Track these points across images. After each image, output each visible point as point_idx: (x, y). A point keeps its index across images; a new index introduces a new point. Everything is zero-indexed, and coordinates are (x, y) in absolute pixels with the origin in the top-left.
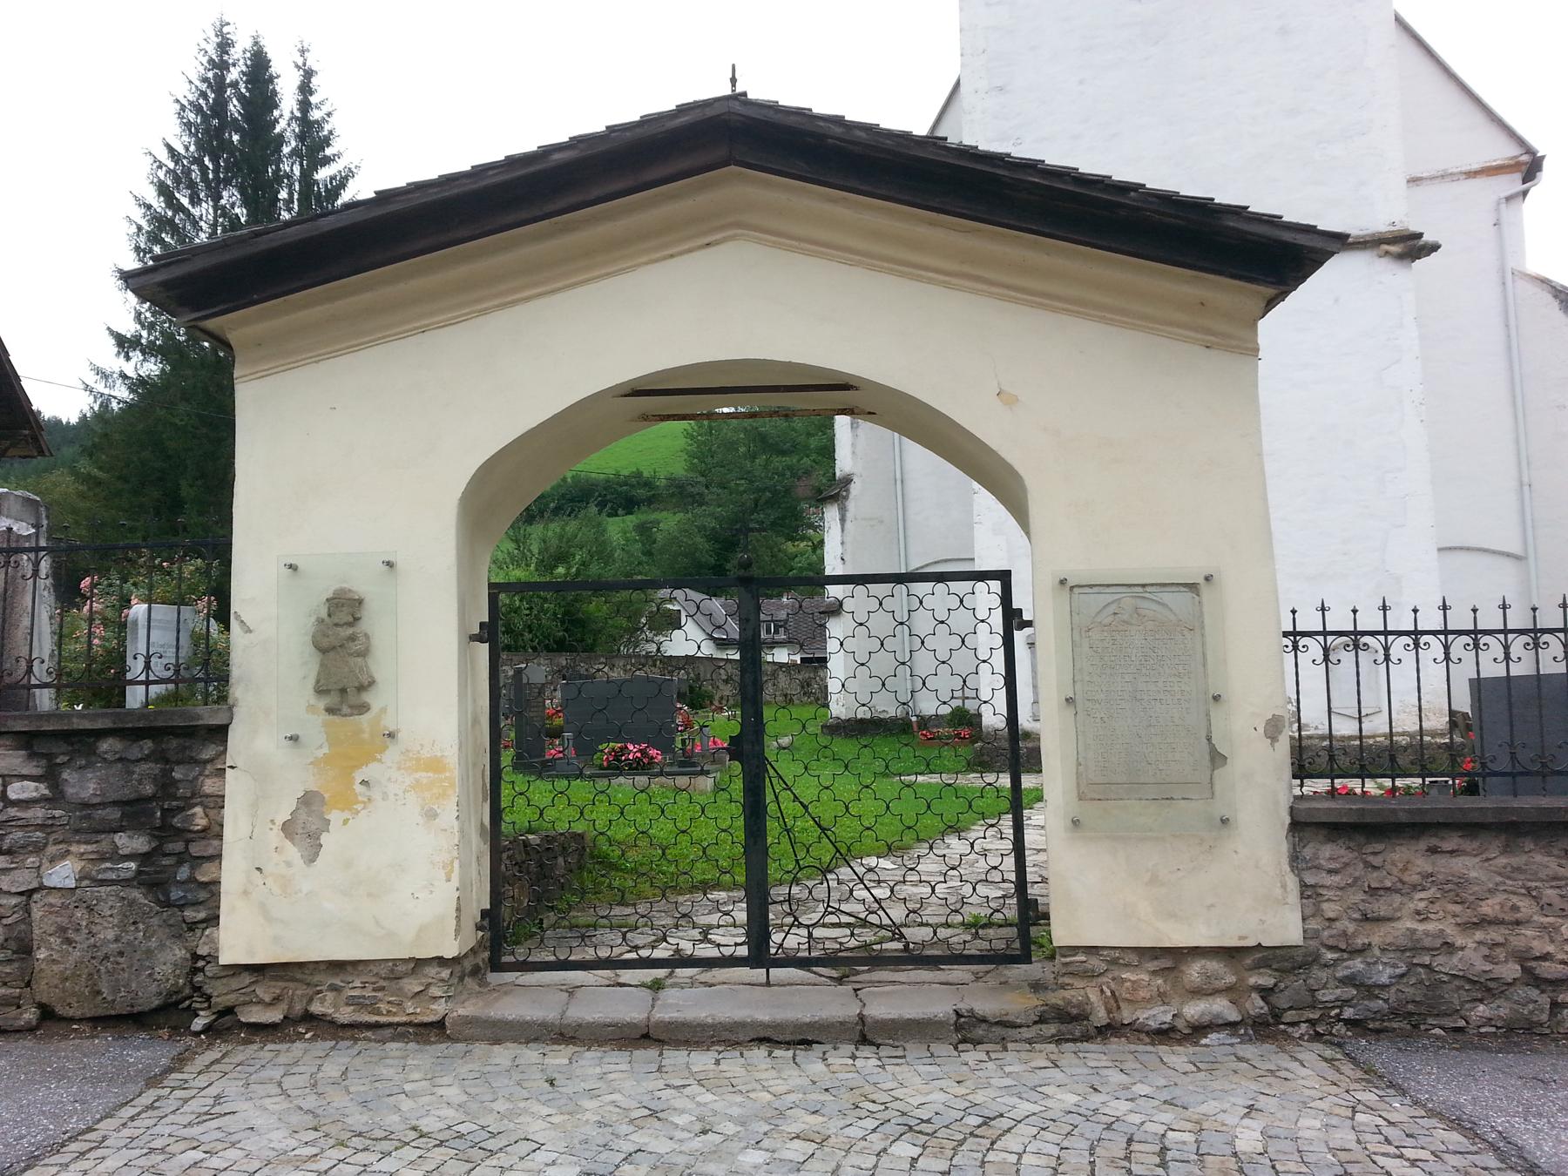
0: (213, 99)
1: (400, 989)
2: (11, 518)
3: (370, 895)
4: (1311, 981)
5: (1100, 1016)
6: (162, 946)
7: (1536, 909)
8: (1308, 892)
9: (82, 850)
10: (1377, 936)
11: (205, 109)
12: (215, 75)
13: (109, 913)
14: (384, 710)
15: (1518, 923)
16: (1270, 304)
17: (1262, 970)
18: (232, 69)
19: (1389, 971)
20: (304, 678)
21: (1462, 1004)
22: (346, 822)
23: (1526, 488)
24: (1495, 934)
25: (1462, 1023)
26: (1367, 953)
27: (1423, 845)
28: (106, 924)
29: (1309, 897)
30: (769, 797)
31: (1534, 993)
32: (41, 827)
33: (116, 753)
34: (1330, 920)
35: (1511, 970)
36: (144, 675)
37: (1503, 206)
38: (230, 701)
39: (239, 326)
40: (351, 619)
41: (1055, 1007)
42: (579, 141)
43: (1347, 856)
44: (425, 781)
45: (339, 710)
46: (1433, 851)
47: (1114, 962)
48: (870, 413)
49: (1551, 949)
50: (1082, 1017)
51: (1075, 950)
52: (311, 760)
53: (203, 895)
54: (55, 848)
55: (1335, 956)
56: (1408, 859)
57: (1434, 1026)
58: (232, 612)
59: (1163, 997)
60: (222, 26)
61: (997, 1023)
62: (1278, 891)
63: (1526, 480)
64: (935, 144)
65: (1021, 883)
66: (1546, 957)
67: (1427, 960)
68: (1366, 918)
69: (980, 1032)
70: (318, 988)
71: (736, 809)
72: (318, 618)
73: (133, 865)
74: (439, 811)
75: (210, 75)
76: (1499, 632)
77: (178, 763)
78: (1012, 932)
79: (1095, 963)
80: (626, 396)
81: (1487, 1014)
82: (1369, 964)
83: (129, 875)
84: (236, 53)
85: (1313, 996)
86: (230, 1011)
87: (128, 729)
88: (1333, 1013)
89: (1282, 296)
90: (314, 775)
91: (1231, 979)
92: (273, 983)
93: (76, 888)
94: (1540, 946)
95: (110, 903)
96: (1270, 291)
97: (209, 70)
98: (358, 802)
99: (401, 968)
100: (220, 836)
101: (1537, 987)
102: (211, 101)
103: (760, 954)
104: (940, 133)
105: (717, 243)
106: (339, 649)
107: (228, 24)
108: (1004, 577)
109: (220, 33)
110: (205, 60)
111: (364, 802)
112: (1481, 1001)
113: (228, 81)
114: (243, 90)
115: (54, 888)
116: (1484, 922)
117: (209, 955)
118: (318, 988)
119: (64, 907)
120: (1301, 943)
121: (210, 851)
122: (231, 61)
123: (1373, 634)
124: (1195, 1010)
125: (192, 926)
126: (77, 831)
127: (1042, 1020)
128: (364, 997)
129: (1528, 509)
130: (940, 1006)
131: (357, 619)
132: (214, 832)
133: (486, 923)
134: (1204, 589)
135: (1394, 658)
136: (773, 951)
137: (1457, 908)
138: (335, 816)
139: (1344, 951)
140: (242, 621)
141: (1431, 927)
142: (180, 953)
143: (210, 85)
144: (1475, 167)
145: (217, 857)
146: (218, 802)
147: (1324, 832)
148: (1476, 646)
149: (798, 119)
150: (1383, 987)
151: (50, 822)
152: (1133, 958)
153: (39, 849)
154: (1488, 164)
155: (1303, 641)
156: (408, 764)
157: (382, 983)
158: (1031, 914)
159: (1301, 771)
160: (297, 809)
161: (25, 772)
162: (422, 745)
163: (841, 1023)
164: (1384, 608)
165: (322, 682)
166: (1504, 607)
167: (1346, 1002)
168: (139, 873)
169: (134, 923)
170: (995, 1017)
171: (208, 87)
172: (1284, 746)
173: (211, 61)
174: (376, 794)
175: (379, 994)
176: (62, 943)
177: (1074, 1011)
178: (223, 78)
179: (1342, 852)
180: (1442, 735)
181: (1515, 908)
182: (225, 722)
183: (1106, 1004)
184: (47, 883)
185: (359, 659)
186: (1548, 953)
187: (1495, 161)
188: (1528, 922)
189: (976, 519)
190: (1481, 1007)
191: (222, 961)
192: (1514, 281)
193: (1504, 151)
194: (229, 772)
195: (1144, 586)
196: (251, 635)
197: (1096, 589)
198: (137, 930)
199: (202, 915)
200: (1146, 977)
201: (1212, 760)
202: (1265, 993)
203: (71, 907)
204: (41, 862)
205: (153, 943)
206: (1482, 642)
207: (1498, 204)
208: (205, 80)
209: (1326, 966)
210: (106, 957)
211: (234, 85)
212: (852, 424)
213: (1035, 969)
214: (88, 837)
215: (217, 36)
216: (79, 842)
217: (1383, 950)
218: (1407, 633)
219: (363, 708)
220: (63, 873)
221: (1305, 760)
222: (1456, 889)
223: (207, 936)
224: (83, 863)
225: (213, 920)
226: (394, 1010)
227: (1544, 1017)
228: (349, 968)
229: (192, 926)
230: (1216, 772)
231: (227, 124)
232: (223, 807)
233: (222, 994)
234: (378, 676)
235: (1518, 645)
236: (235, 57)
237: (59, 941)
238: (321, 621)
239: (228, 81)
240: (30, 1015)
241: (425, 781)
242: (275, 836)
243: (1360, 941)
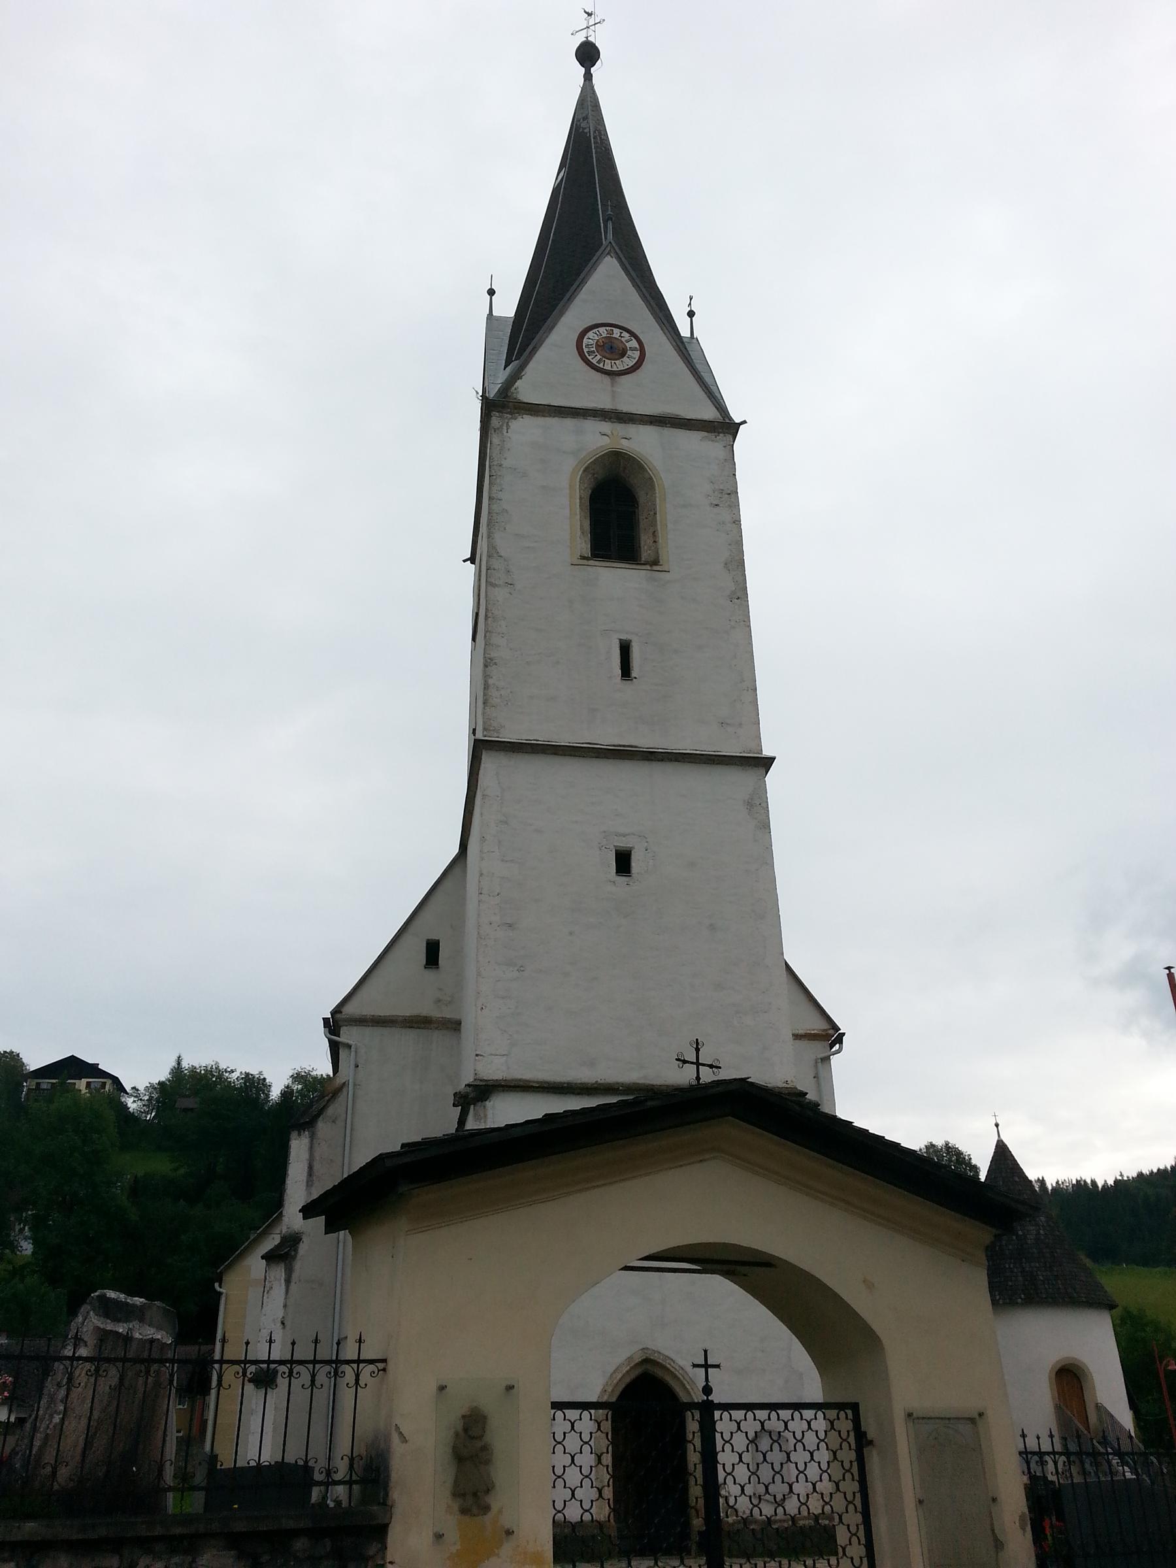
2: (153, 1327)
14: (500, 1511)
37: (820, 1065)
108: (855, 1407)
140: (401, 1432)
154: (808, 1032)
187: (814, 1030)
193: (818, 1025)
195: (949, 1419)
201: (996, 1547)
206: (340, 1370)
212: (307, 1182)
219: (486, 1509)
235: (323, 1371)
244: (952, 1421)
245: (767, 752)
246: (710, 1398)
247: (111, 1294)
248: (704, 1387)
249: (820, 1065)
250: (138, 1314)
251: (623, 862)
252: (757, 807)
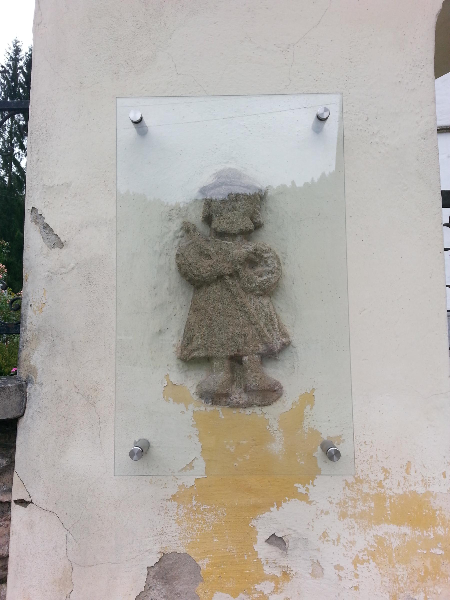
0: (12, 74)
11: (8, 78)
12: (13, 64)
18: (20, 61)
20: (161, 332)
38: (22, 373)
40: (251, 226)
44: (395, 542)
45: (227, 395)
58: (28, 207)
60: (16, 43)
72: (185, 223)
75: (11, 63)
84: (22, 54)
90: (178, 522)
97: (10, 61)
98: (264, 578)
102: (11, 74)
106: (228, 280)
107: (19, 42)
109: (15, 46)
110: (9, 57)
111: (274, 578)
113: (18, 66)
114: (25, 71)
122: (20, 58)
131: (258, 226)
140: (46, 226)
143: (10, 68)
156: (361, 507)
160: (148, 588)
162: (386, 471)
165: (197, 341)
171: (10, 68)
173: (11, 57)
178: (16, 65)
182: (11, 415)
185: (265, 301)
194: (16, 511)
196: (64, 251)
208: (8, 65)
211: (21, 68)
215: (14, 47)
231: (18, 84)
234: (294, 339)
236: (22, 56)
239: (18, 66)
241: (395, 542)
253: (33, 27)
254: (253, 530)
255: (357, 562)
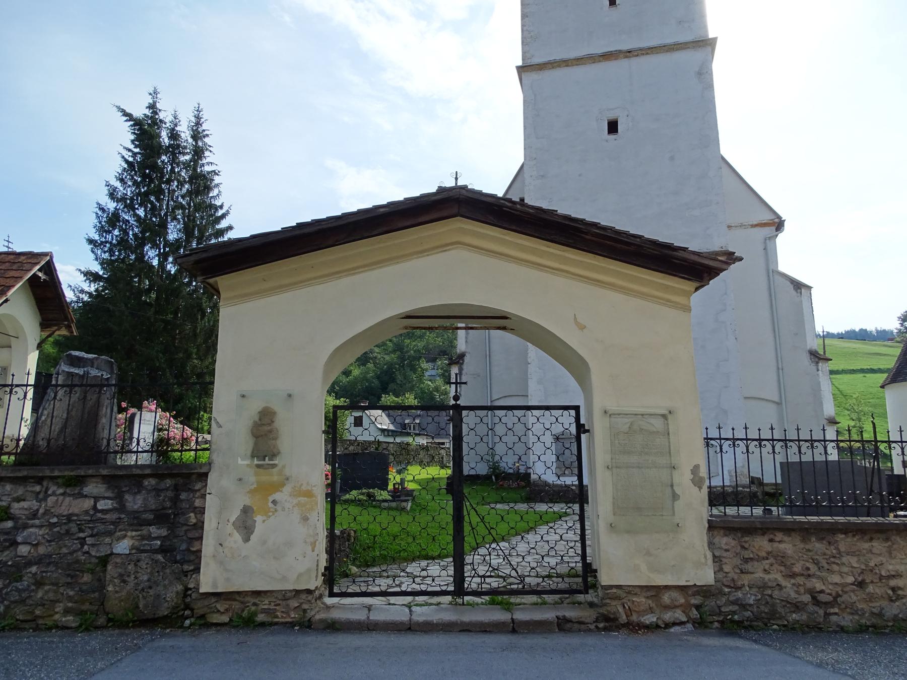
1: (288, 605)
3: (274, 558)
4: (718, 602)
5: (623, 619)
6: (171, 583)
7: (816, 568)
8: (717, 559)
9: (133, 535)
10: (746, 580)
13: (145, 567)
14: (284, 467)
15: (809, 576)
16: (697, 289)
17: (696, 597)
19: (753, 597)
21: (786, 613)
22: (264, 521)
23: (781, 371)
24: (800, 580)
25: (786, 623)
26: (743, 589)
27: (766, 537)
28: (143, 572)
29: (717, 562)
30: (465, 513)
31: (816, 608)
32: (113, 523)
33: (152, 486)
34: (726, 573)
35: (807, 598)
36: (195, 447)
39: (223, 282)
41: (603, 615)
42: (392, 204)
43: (733, 543)
46: (771, 541)
47: (629, 593)
48: (512, 329)
49: (824, 588)
50: (615, 619)
51: (611, 587)
52: (248, 490)
53: (192, 557)
54: (119, 533)
55: (730, 590)
56: (761, 544)
57: (774, 624)
59: (651, 610)
61: (577, 622)
62: (703, 560)
63: (780, 367)
64: (552, 213)
65: (584, 556)
66: (822, 592)
67: (769, 592)
68: (742, 572)
69: (568, 625)
70: (247, 604)
71: (450, 519)
73: (159, 542)
74: (309, 517)
76: (796, 440)
77: (183, 491)
78: (580, 580)
79: (619, 592)
80: (403, 318)
81: (797, 618)
82: (744, 594)
83: (157, 547)
85: (720, 610)
86: (203, 616)
87: (159, 474)
88: (728, 617)
89: (703, 286)
91: (682, 601)
92: (224, 602)
93: (130, 554)
94: (819, 586)
95: (146, 562)
96: (696, 284)
99: (289, 594)
100: (202, 528)
101: (818, 606)
103: (459, 590)
104: (508, 196)
105: (449, 250)
108: (577, 408)
112: (794, 612)
115: (118, 554)
116: (793, 575)
117: (194, 588)
118: (247, 604)
119: (123, 564)
120: (713, 583)
121: (197, 535)
123: (819, 441)
124: (668, 616)
125: (186, 574)
126: (132, 525)
127: (597, 621)
128: (270, 609)
129: (782, 380)
130: (549, 615)
131: (273, 422)
132: (199, 526)
133: (327, 573)
134: (669, 417)
135: (724, 450)
136: (466, 586)
137: (782, 568)
138: (259, 519)
139: (732, 588)
141: (771, 576)
142: (180, 588)
144: (755, 223)
145: (201, 538)
146: (202, 511)
147: (722, 532)
148: (760, 446)
149: (494, 200)
150: (751, 605)
151: (118, 521)
152: (637, 590)
153: (110, 534)
155: (816, 444)
156: (295, 493)
157: (278, 602)
158: (589, 570)
159: (712, 503)
161: (106, 495)
163: (503, 622)
164: (746, 428)
166: (772, 429)
167: (734, 613)
168: (161, 545)
169: (158, 572)
170: (575, 618)
172: (705, 490)
174: (279, 507)
175: (277, 608)
176: (121, 582)
177: (612, 616)
179: (731, 540)
180: (747, 488)
181: (808, 569)
183: (626, 613)
184: (114, 551)
185: (274, 441)
186: (823, 590)
188: (814, 575)
189: (529, 376)
190: (794, 615)
191: (201, 591)
192: (773, 276)
194: (208, 495)
197: (621, 416)
198: (159, 575)
199: (192, 568)
200: (644, 600)
202: (698, 607)
203: (127, 564)
204: (112, 540)
205: (166, 582)
207: (766, 240)
209: (724, 594)
210: (143, 590)
213: (590, 597)
214: (136, 528)
216: (132, 531)
217: (750, 588)
218: (756, 440)
220: (123, 546)
221: (717, 498)
222: (781, 559)
223: (194, 578)
224: (134, 541)
225: (197, 570)
226: (285, 616)
227: (822, 620)
228: (263, 594)
229: (186, 574)
230: (675, 502)
232: (204, 513)
233: (200, 607)
235: (804, 446)
237: (119, 581)
238: (255, 422)
240: (102, 621)
242: (230, 528)
243: (739, 583)
244: (644, 416)
245: (711, 36)
246: (458, 402)
247: (77, 353)
248: (454, 396)
249: (768, 241)
250: (91, 363)
251: (613, 127)
252: (704, 76)
253: (702, 16)
254: (268, 500)
255: (293, 507)
